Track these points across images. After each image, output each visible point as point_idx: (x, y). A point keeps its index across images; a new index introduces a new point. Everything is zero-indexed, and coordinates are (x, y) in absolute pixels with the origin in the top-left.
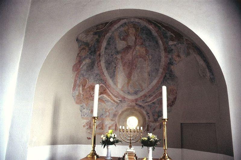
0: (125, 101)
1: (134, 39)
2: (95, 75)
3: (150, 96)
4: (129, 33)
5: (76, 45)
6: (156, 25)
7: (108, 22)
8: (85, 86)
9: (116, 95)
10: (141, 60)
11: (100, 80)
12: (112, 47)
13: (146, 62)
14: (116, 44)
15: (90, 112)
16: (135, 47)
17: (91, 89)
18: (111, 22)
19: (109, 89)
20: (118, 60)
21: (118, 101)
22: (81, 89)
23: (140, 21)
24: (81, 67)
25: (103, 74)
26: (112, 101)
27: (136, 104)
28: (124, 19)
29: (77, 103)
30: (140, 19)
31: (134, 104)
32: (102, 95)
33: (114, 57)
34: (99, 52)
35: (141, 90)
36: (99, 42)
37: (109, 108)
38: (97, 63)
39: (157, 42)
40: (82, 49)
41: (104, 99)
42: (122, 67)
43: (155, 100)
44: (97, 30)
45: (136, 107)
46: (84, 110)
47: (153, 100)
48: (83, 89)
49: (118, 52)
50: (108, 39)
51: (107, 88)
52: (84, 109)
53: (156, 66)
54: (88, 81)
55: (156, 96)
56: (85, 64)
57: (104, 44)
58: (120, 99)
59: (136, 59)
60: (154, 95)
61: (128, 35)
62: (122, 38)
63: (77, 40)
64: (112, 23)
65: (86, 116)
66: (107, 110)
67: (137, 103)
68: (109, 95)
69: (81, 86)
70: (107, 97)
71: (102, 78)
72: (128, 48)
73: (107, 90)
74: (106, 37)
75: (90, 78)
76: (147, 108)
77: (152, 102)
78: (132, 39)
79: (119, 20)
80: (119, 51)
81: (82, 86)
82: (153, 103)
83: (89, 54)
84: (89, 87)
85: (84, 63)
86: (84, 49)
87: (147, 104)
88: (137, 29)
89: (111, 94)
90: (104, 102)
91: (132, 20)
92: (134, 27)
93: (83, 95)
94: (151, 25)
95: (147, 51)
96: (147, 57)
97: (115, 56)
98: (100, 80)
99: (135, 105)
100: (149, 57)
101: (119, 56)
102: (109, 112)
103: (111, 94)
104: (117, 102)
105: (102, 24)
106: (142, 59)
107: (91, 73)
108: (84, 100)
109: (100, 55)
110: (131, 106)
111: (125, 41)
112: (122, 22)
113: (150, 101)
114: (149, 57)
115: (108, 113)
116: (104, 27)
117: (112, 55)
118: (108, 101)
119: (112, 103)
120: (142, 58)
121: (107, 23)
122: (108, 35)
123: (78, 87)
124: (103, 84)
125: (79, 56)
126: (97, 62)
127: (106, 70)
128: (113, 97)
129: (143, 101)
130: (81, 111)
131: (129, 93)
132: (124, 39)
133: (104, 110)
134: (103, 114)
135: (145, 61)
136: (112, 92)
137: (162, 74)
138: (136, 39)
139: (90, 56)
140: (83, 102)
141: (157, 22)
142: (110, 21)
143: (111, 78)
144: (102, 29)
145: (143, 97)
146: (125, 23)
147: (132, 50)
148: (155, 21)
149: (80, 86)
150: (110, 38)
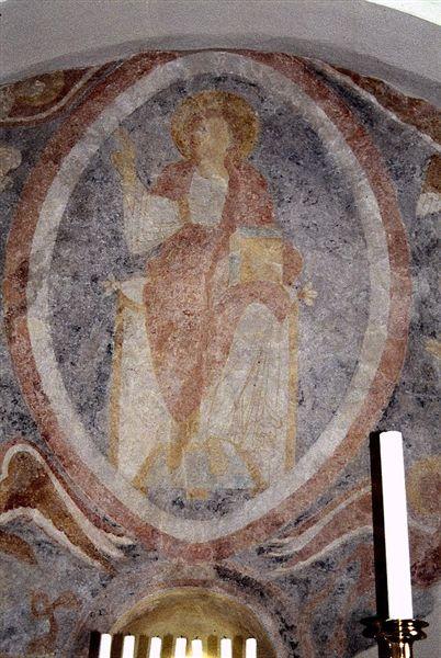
0: (151, 554)
3: (303, 521)
4: (200, 150)
6: (348, 102)
7: (85, 71)
9: (102, 512)
10: (256, 316)
11: (15, 418)
12: (99, 232)
13: (287, 322)
14: (121, 215)
16: (228, 236)
18: (98, 74)
21: (116, 554)
23: (261, 72)
26: (77, 550)
27: (218, 569)
28: (171, 56)
30: (266, 57)
31: (206, 569)
32: (19, 511)
33: (108, 293)
34: (19, 254)
35: (252, 486)
37: (54, 595)
39: (350, 207)
41: (29, 539)
42: (148, 350)
43: (329, 547)
44: (53, 543)
45: (220, 593)
47: (321, 545)
49: (128, 265)
50: (73, 181)
51: (55, 471)
53: (339, 347)
55: (336, 523)
58: (126, 541)
59: (230, 309)
60: (327, 518)
61: (188, 164)
62: (155, 176)
64: (106, 79)
66: (41, 607)
67: (230, 563)
68: (61, 517)
70: (48, 524)
72: (190, 238)
73: (57, 484)
74: (65, 165)
76: (284, 595)
77: (314, 558)
78: (212, 181)
79: (149, 58)
80: (138, 257)
82: (322, 564)
87: (281, 570)
88: (245, 129)
89: (72, 508)
91: (219, 64)
92: (226, 114)
94: (324, 97)
95: (292, 264)
96: (292, 292)
97: (109, 286)
98: (15, 418)
99: (212, 574)
100: (301, 295)
101: (133, 289)
103: (72, 508)
104: (105, 560)
105: (45, 78)
106: (264, 307)
109: (23, 273)
110: (188, 583)
113: (302, 555)
114: (301, 295)
115: (45, 625)
116: (58, 99)
117: (95, 279)
118: (51, 547)
119: (81, 565)
120: (264, 301)
121: (72, 76)
122: (80, 155)
124: (34, 446)
128: (86, 525)
129: (261, 551)
131: (182, 505)
132: (166, 189)
133: (25, 605)
134: (11, 631)
135: (281, 318)
136: (81, 492)
137: (373, 392)
138: (233, 184)
141: (356, 78)
142: (96, 65)
143: (81, 409)
144: (43, 108)
145: (260, 530)
146: (178, 87)
147: (207, 258)
148: (345, 72)
150: (88, 175)
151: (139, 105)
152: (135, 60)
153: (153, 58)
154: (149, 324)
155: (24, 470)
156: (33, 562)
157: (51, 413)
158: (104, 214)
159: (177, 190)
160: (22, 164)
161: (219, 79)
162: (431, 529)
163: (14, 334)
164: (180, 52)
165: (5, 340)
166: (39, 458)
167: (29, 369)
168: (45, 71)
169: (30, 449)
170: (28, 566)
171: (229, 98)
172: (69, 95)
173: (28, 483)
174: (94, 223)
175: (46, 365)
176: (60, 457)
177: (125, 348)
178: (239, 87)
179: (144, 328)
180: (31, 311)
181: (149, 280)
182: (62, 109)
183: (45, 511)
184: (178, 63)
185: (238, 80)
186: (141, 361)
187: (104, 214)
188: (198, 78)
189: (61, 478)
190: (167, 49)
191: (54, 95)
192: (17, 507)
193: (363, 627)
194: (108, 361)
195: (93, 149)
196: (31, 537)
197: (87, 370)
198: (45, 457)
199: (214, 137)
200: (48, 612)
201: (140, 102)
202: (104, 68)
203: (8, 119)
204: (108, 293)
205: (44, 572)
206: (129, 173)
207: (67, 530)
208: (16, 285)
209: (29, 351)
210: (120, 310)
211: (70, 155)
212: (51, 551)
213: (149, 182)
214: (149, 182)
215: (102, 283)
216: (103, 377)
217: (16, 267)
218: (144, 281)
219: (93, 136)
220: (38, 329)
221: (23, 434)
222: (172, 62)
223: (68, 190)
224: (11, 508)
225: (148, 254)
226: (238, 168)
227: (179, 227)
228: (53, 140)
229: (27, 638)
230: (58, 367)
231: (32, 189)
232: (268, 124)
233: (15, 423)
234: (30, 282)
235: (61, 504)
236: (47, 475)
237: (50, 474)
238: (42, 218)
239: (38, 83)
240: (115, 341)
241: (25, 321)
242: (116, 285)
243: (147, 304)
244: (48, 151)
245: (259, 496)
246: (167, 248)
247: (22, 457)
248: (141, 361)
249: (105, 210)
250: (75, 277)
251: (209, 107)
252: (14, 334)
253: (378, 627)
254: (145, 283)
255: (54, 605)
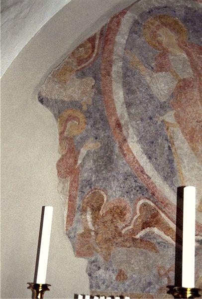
1: (185, 56)
2: (121, 178)
4: (164, 46)
5: (46, 114)
8: (99, 210)
11: (138, 188)
15: (114, 278)
17: (116, 215)
18: (101, 34)
19: (167, 210)
20: (171, 128)
22: (89, 217)
24: (79, 162)
25: (142, 171)
28: (123, 13)
29: (79, 254)
32: (148, 230)
33: (159, 123)
34: (113, 118)
36: (102, 92)
38: (120, 147)
40: (67, 121)
46: (101, 272)
48: (95, 219)
52: (99, 268)
54: (105, 196)
56: (87, 155)
57: (119, 95)
61: (164, 53)
62: (153, 64)
63: (41, 101)
65: (104, 286)
66: (162, 272)
69: (89, 209)
70: (162, 233)
71: (140, 182)
73: (163, 215)
74: (113, 75)
75: (111, 188)
79: (116, 18)
80: (165, 102)
81: (93, 210)
83: (89, 127)
84: (111, 211)
85: (83, 151)
86: (71, 118)
90: (154, 248)
93: (97, 233)
97: (159, 120)
102: (168, 278)
105: (81, 46)
107: (110, 174)
108: (99, 244)
109: (119, 125)
111: (166, 71)
112: (126, 22)
116: (93, 51)
121: (92, 40)
122: (117, 68)
123: (80, 213)
124: (149, 199)
125: (64, 138)
126: (117, 145)
127: (148, 160)
130: (90, 275)
132: (161, 68)
133: (155, 271)
138: (188, 54)
139: (95, 132)
140: (97, 251)
143: (166, 179)
144: (90, 57)
146: (136, 23)
149: (84, 211)
150: (125, 76)
151: (126, 38)
152: (111, 21)
153: (117, 17)
154: (183, 132)
155: (147, 210)
156: (157, 252)
157: (152, 183)
158: (141, 89)
159: (166, 67)
160: (96, 83)
161: (149, 12)
162: (200, 238)
163: (125, 152)
164: (126, 9)
165: (122, 156)
166: (152, 204)
167: (137, 166)
168: (79, 43)
169: (147, 201)
170: (155, 254)
171: (160, 17)
172: (96, 47)
173: (150, 216)
174: (139, 95)
175: (143, 161)
176: (161, 202)
177: (176, 146)
178: (160, 10)
179: (181, 134)
180: (129, 140)
181: (175, 111)
182: (97, 54)
183: (168, 225)
184: (129, 14)
185: (158, 8)
186: (186, 150)
187: (141, 89)
188: (141, 16)
189: (164, 212)
190: (120, 10)
191: (90, 51)
192: (147, 228)
193: (168, 289)
194: (171, 153)
195: (121, 64)
196: (155, 241)
197: (163, 160)
198: (155, 203)
199: (166, 37)
200: (166, 274)
201: (126, 37)
202: (102, 31)
203: (79, 67)
204: (159, 123)
205: (162, 256)
206: (141, 67)
207: (171, 235)
208: (118, 131)
209: (134, 158)
210: (168, 129)
211: (113, 70)
212: (165, 246)
213: (152, 68)
214: (152, 68)
215: (155, 119)
216: (171, 161)
217: (114, 124)
218: (172, 113)
219: (117, 59)
220: (135, 148)
221: (143, 195)
222: (126, 15)
223: (120, 85)
224: (144, 228)
225: (169, 100)
226: (186, 46)
227: (176, 83)
228: (102, 67)
229: (157, 287)
230: (150, 162)
231: (106, 90)
232: (185, 20)
233: (138, 191)
234: (123, 129)
235: (167, 223)
236: (157, 211)
237: (159, 210)
238: (116, 100)
239: (80, 49)
240: (171, 143)
241: (128, 146)
242: (161, 118)
243: (179, 123)
244: (103, 72)
245: (67, 237)
246: (176, 94)
247: (145, 205)
248: (186, 150)
249: (141, 87)
250: (142, 120)
251: (155, 25)
252: (125, 152)
253: (176, 288)
254: (174, 113)
255: (168, 271)
